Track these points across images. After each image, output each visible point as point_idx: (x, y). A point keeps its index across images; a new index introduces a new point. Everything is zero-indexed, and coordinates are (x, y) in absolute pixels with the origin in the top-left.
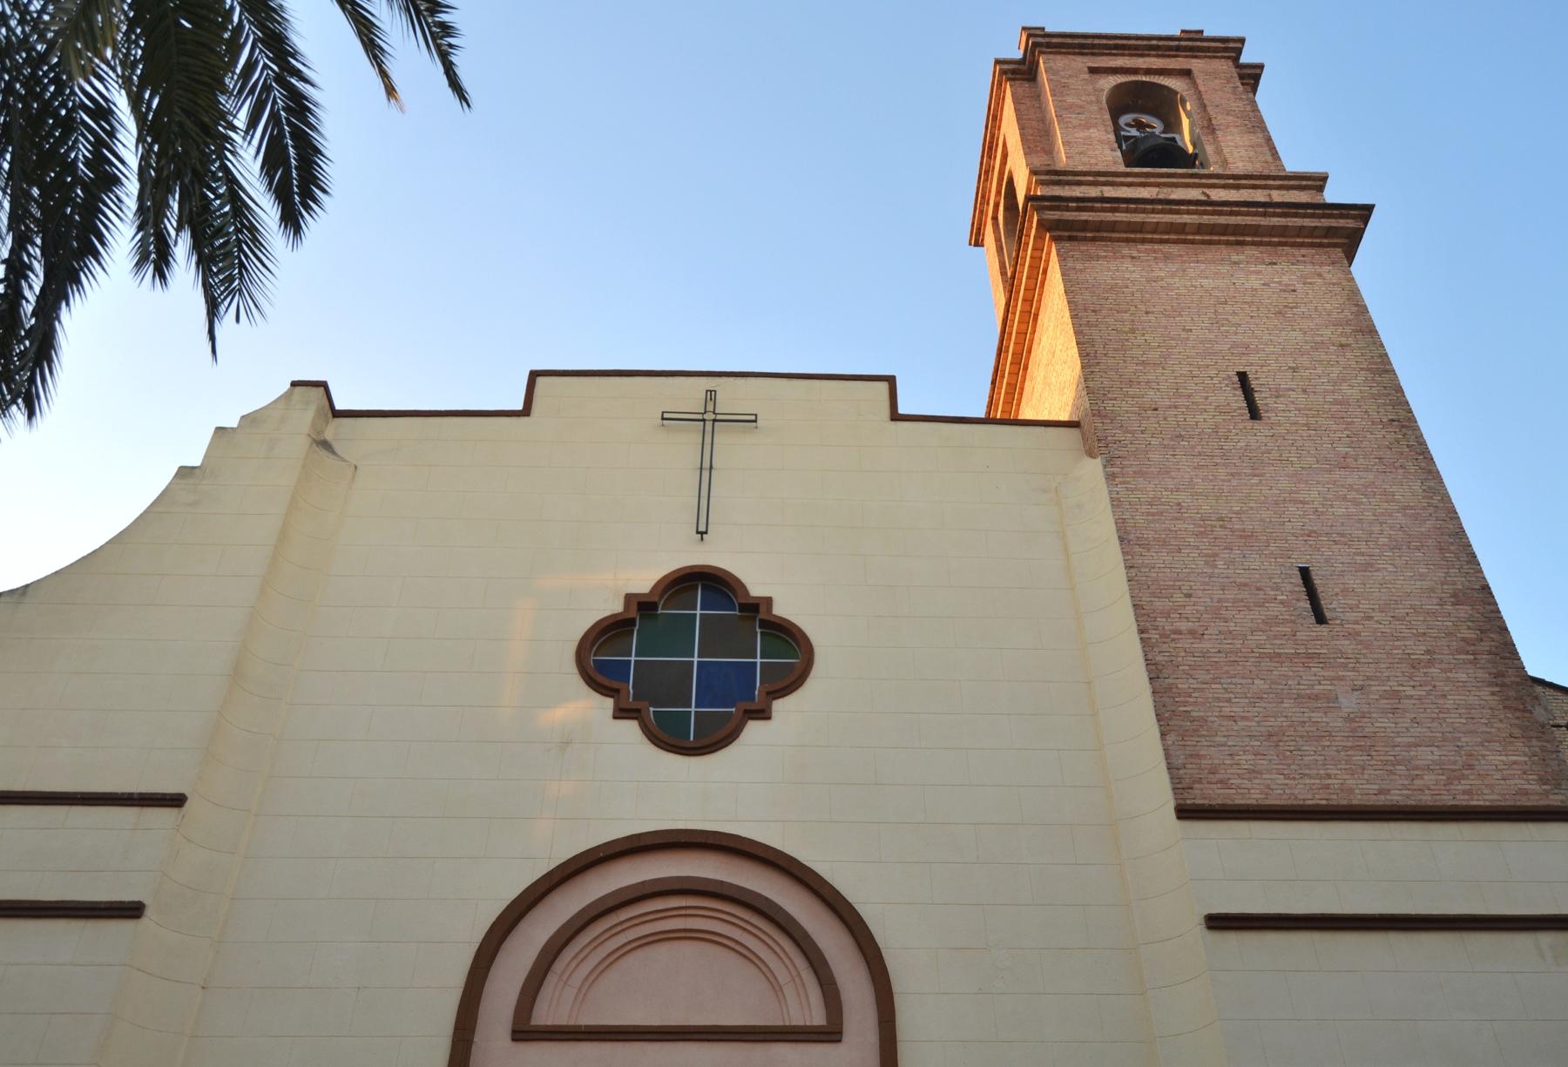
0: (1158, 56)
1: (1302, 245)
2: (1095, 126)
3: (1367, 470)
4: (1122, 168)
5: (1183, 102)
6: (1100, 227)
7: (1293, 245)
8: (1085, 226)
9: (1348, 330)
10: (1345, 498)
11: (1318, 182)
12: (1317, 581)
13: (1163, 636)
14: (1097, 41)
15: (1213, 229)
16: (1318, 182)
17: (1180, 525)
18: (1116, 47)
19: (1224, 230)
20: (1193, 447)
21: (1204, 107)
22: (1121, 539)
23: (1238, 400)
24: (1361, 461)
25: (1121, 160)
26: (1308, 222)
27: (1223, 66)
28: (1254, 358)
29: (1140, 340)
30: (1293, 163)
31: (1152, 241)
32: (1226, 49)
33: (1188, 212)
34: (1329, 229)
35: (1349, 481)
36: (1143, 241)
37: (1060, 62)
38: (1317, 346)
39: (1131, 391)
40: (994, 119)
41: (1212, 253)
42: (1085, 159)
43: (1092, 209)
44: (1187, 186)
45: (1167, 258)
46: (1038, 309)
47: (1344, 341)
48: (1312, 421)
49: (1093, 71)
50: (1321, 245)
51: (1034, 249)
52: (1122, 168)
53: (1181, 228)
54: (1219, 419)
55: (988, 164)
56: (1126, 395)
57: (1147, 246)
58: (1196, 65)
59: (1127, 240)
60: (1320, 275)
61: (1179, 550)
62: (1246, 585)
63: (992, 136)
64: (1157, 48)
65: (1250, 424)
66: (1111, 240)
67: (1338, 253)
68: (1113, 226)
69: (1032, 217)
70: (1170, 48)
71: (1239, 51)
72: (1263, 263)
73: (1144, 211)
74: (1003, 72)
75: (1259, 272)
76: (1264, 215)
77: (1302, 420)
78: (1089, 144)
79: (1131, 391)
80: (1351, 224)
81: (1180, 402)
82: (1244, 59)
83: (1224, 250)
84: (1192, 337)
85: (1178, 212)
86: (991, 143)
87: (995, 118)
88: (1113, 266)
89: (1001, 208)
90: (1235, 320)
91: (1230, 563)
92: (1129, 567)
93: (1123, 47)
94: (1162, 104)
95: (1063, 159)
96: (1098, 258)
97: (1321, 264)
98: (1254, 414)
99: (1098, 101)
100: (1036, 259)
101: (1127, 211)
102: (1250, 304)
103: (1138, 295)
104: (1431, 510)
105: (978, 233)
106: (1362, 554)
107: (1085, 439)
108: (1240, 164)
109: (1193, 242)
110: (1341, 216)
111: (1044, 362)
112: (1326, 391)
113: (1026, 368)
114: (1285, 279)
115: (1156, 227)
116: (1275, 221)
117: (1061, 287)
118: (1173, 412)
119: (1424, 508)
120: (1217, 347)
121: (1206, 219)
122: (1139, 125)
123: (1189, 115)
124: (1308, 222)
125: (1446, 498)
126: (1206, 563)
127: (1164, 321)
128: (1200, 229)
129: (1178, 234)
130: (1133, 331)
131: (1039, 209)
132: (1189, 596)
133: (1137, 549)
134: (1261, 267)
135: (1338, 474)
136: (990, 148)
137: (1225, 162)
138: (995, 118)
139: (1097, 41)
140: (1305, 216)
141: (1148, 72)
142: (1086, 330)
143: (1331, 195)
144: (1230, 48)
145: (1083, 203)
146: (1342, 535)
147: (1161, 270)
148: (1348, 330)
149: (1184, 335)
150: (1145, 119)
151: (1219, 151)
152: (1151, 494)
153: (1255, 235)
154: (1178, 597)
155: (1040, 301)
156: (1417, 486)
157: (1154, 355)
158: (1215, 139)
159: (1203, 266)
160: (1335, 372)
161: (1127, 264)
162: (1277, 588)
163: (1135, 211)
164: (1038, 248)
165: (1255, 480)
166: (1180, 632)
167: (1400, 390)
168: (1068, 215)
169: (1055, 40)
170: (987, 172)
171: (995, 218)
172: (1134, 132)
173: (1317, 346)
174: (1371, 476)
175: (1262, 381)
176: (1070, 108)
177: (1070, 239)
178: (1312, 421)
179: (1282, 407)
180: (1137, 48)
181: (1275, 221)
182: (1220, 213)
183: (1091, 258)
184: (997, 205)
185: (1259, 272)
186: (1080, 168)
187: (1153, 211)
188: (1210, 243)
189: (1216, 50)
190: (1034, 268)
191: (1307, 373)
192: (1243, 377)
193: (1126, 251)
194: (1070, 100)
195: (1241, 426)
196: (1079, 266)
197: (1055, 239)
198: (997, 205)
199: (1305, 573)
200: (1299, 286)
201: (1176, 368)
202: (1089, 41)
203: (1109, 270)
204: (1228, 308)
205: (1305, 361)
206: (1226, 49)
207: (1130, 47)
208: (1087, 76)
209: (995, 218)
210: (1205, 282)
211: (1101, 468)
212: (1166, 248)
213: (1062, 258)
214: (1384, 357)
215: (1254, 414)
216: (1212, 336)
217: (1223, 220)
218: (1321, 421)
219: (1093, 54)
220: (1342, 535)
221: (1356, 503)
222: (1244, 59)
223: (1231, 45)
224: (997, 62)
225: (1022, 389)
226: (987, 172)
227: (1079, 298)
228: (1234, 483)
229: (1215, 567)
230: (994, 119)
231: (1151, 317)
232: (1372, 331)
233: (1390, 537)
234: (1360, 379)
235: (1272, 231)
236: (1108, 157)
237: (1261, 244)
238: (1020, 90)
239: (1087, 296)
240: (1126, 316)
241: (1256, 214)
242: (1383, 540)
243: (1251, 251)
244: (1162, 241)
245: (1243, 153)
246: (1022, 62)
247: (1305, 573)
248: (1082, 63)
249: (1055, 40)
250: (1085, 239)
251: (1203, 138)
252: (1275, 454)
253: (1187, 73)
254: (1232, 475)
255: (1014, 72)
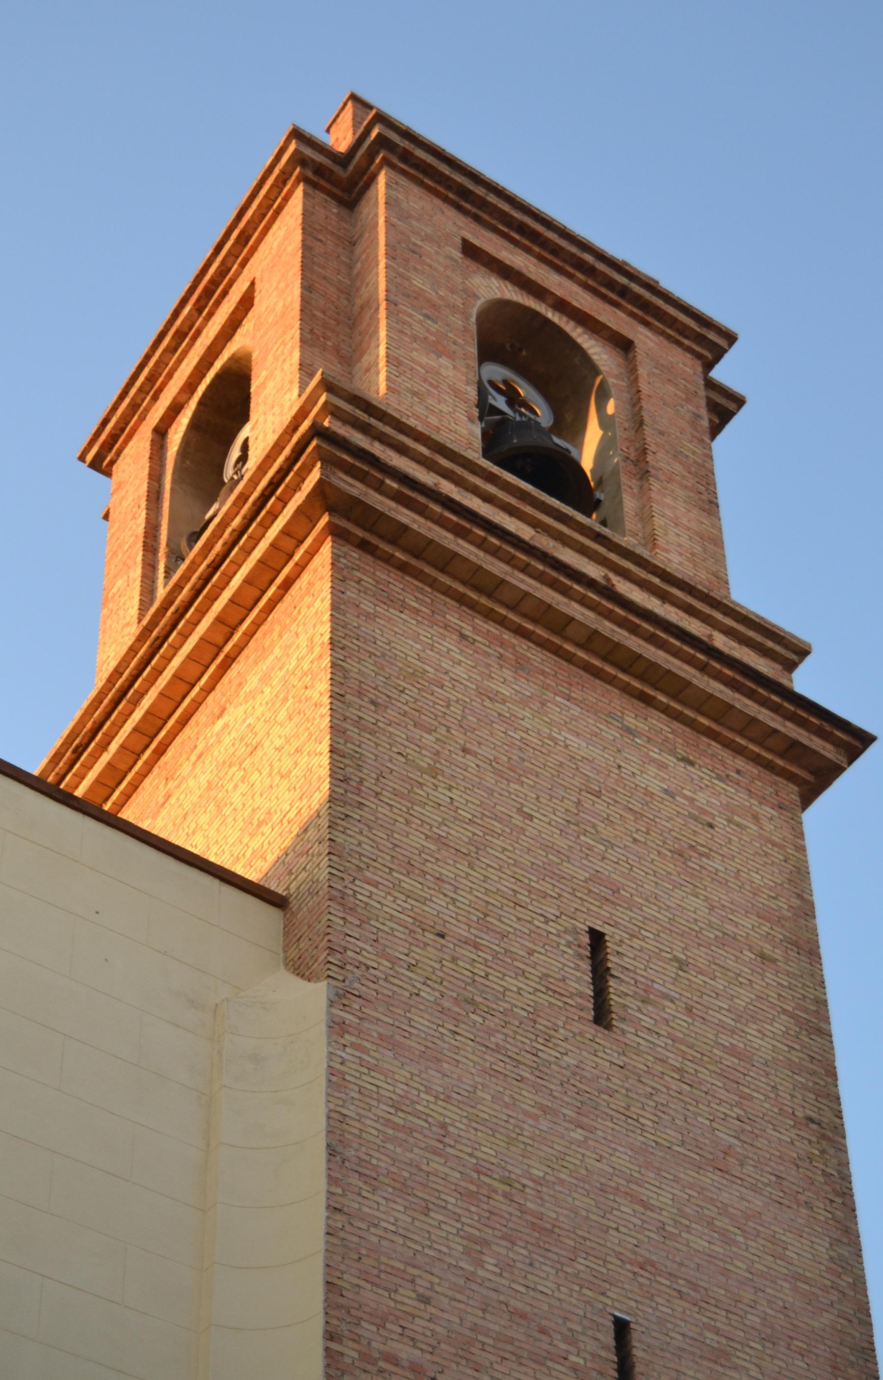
0: (586, 287)
1: (739, 751)
2: (451, 356)
3: (754, 1188)
4: (475, 455)
5: (603, 396)
6: (423, 549)
7: (728, 745)
8: (398, 534)
9: (778, 933)
10: (710, 1224)
11: (794, 652)
12: (638, 1353)
13: (364, 1356)
14: (492, 198)
15: (612, 652)
16: (794, 652)
17: (437, 1165)
18: (522, 229)
19: (631, 663)
20: (490, 1032)
21: (640, 424)
22: (332, 1152)
23: (580, 981)
24: (749, 1169)
25: (478, 443)
26: (765, 716)
27: (683, 363)
28: (622, 915)
29: (442, 795)
30: (747, 592)
31: (502, 622)
32: (700, 339)
33: (583, 601)
34: (795, 744)
35: (724, 1197)
36: (489, 615)
37: (417, 200)
38: (726, 940)
39: (408, 883)
40: (242, 238)
41: (596, 692)
42: (419, 410)
43: (422, 511)
44: (583, 551)
45: (520, 665)
46: (240, 649)
47: (768, 949)
48: (690, 1067)
49: (470, 250)
50: (769, 766)
51: (285, 532)
52: (475, 455)
53: (561, 624)
54: (544, 999)
55: (190, 322)
56: (397, 885)
57: (492, 628)
58: (645, 339)
59: (461, 600)
60: (756, 818)
61: (426, 1211)
62: (524, 1316)
63: (223, 272)
64: (591, 271)
65: (591, 1030)
66: (433, 584)
67: (792, 792)
68: (447, 561)
69: (307, 469)
70: (611, 284)
71: (719, 354)
72: (673, 752)
73: (510, 561)
74: (298, 159)
75: (663, 766)
76: (703, 668)
77: (675, 1060)
78: (435, 390)
79: (408, 883)
80: (828, 751)
81: (486, 940)
82: (719, 373)
83: (616, 701)
84: (530, 832)
85: (565, 591)
86: (215, 283)
87: (244, 239)
88: (426, 633)
89: (184, 419)
90: (606, 832)
91: (506, 1266)
92: (334, 1209)
93: (534, 236)
94: (568, 383)
95: (379, 385)
96: (403, 607)
97: (762, 800)
98: (602, 1014)
99: (466, 316)
100: (280, 553)
101: (481, 544)
102: (638, 816)
103: (456, 709)
104: (834, 1296)
105: (108, 445)
106: (717, 1332)
107: (289, 933)
108: (675, 558)
109: (569, 658)
110: (820, 733)
111: (220, 753)
112: (722, 1025)
113: (161, 751)
114: (702, 798)
115: (519, 602)
116: (716, 688)
117: (324, 631)
118: (467, 952)
119: (825, 1288)
120: (567, 868)
121: (607, 628)
122: (513, 398)
123: (605, 422)
124: (765, 716)
125: (859, 1284)
126: (467, 1252)
127: (490, 780)
128: (591, 640)
129: (549, 631)
130: (434, 772)
131: (329, 462)
132: (426, 1301)
133: (354, 1180)
134: (671, 760)
135: (710, 1178)
136: (208, 293)
137: (652, 541)
138: (244, 239)
139: (492, 198)
140: (764, 703)
141: (561, 305)
142: (352, 731)
143: (805, 681)
144: (707, 340)
145: (411, 492)
146: (695, 1287)
147: (506, 684)
148: (778, 933)
149: (518, 820)
150: (524, 390)
151: (645, 516)
152: (401, 1089)
153: (674, 697)
154: (406, 1295)
155: (250, 635)
156: (822, 1247)
157: (459, 834)
158: (643, 493)
159: (576, 711)
160: (744, 997)
161: (450, 644)
162: (572, 1339)
163: (495, 552)
164: (293, 535)
165: (578, 1135)
166: (394, 1360)
167: (832, 1073)
168: (376, 500)
169: (420, 153)
170: (180, 335)
171: (161, 433)
172: (500, 402)
173: (726, 940)
174: (758, 1203)
175: (627, 962)
176: (416, 296)
177: (364, 546)
178: (690, 1067)
179: (648, 1022)
180: (556, 250)
181: (716, 688)
182: (634, 630)
183: (390, 601)
184: (175, 409)
185: (663, 766)
186: (412, 422)
187: (524, 569)
188: (597, 673)
189: (684, 330)
190: (268, 567)
191: (699, 980)
192: (597, 939)
193: (453, 618)
194: (418, 282)
195: (577, 1027)
196: (367, 606)
197: (334, 531)
198: (175, 409)
199: (621, 1328)
200: (720, 821)
201: (492, 874)
202: (480, 191)
203: (416, 638)
204: (600, 806)
205: (700, 956)
206: (700, 339)
207: (544, 243)
208: (457, 255)
209: (161, 433)
210: (575, 742)
211: (323, 1003)
212: (523, 647)
213: (340, 576)
214: (822, 1003)
215: (602, 1014)
216: (563, 844)
217: (634, 643)
218: (704, 1074)
219: (477, 219)
220: (695, 1287)
221: (728, 1241)
222: (719, 373)
223: (712, 336)
224: (296, 134)
225: (134, 787)
226: (180, 335)
227: (352, 666)
228: (544, 1125)
229: (481, 1264)
230: (242, 238)
231: (470, 761)
232: (813, 953)
233: (764, 1318)
234: (778, 1027)
235: (705, 703)
236: (465, 433)
237: (677, 717)
238: (321, 213)
239: (369, 667)
240: (428, 739)
241: (690, 661)
242: (753, 1320)
243: (657, 721)
244: (519, 631)
245: (684, 540)
246: (343, 160)
247: (621, 1328)
248: (456, 225)
249: (420, 153)
250: (388, 560)
251: (624, 479)
252: (619, 1102)
253: (624, 345)
254: (544, 1109)
255: (319, 170)
